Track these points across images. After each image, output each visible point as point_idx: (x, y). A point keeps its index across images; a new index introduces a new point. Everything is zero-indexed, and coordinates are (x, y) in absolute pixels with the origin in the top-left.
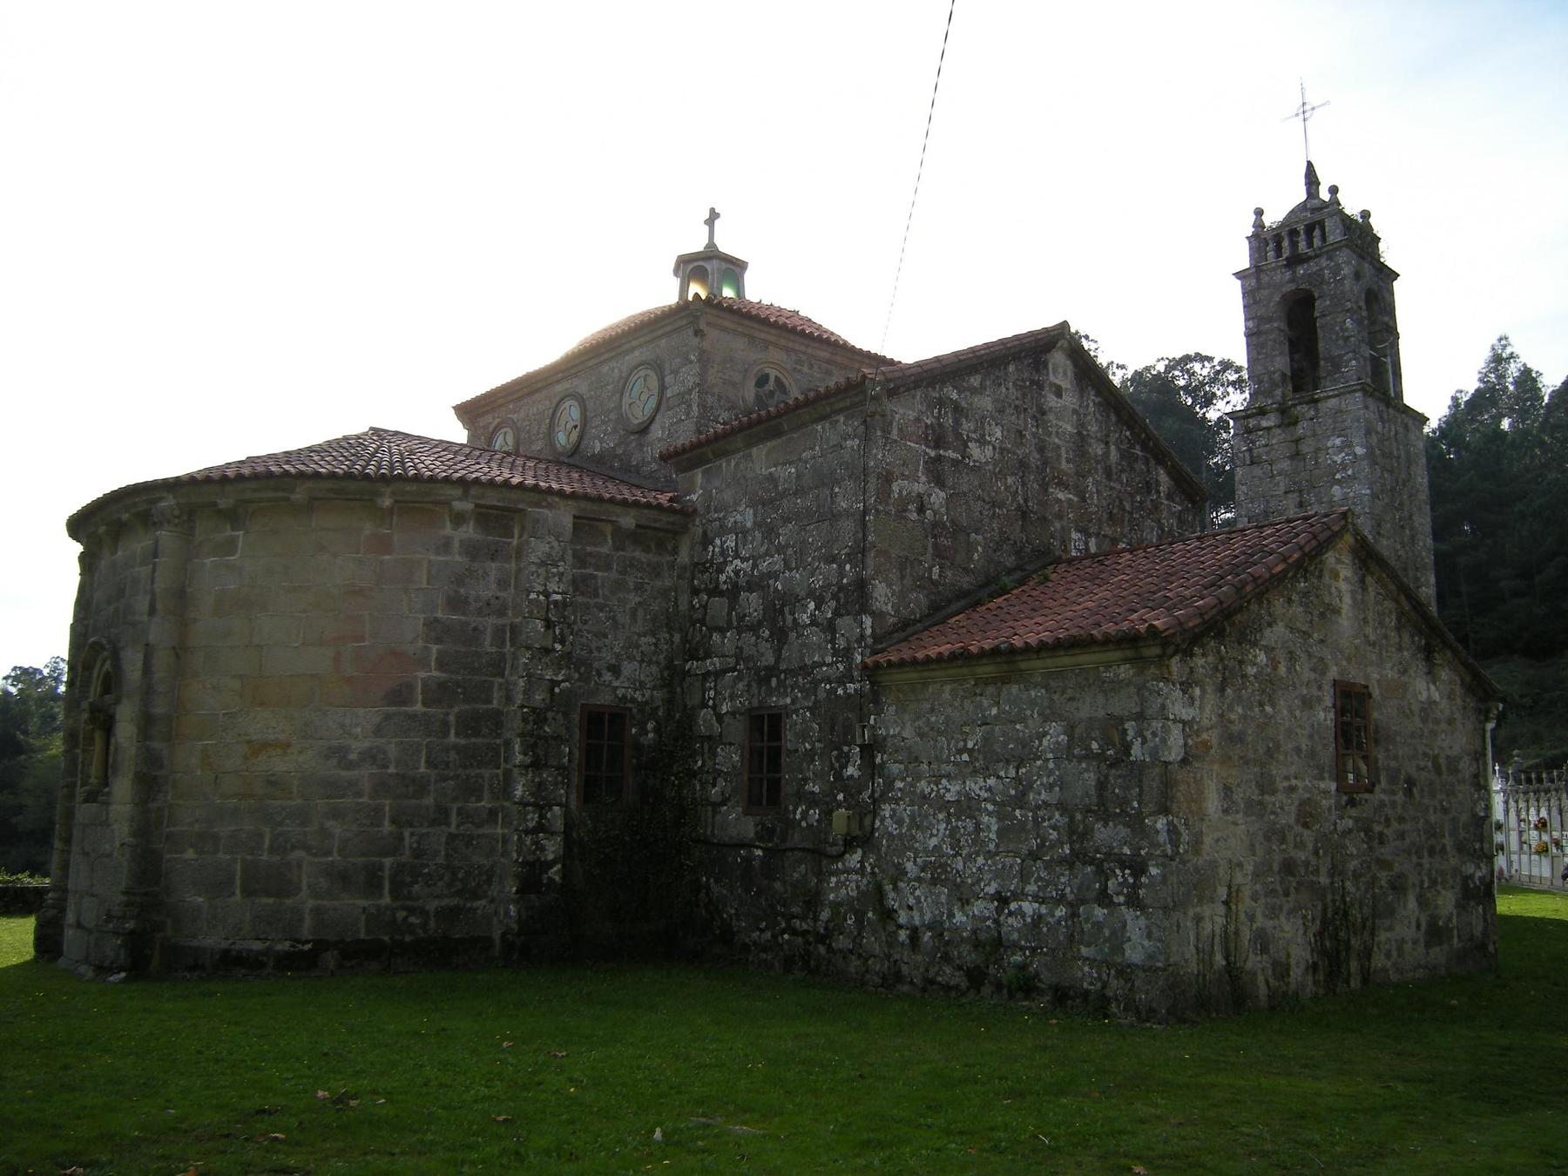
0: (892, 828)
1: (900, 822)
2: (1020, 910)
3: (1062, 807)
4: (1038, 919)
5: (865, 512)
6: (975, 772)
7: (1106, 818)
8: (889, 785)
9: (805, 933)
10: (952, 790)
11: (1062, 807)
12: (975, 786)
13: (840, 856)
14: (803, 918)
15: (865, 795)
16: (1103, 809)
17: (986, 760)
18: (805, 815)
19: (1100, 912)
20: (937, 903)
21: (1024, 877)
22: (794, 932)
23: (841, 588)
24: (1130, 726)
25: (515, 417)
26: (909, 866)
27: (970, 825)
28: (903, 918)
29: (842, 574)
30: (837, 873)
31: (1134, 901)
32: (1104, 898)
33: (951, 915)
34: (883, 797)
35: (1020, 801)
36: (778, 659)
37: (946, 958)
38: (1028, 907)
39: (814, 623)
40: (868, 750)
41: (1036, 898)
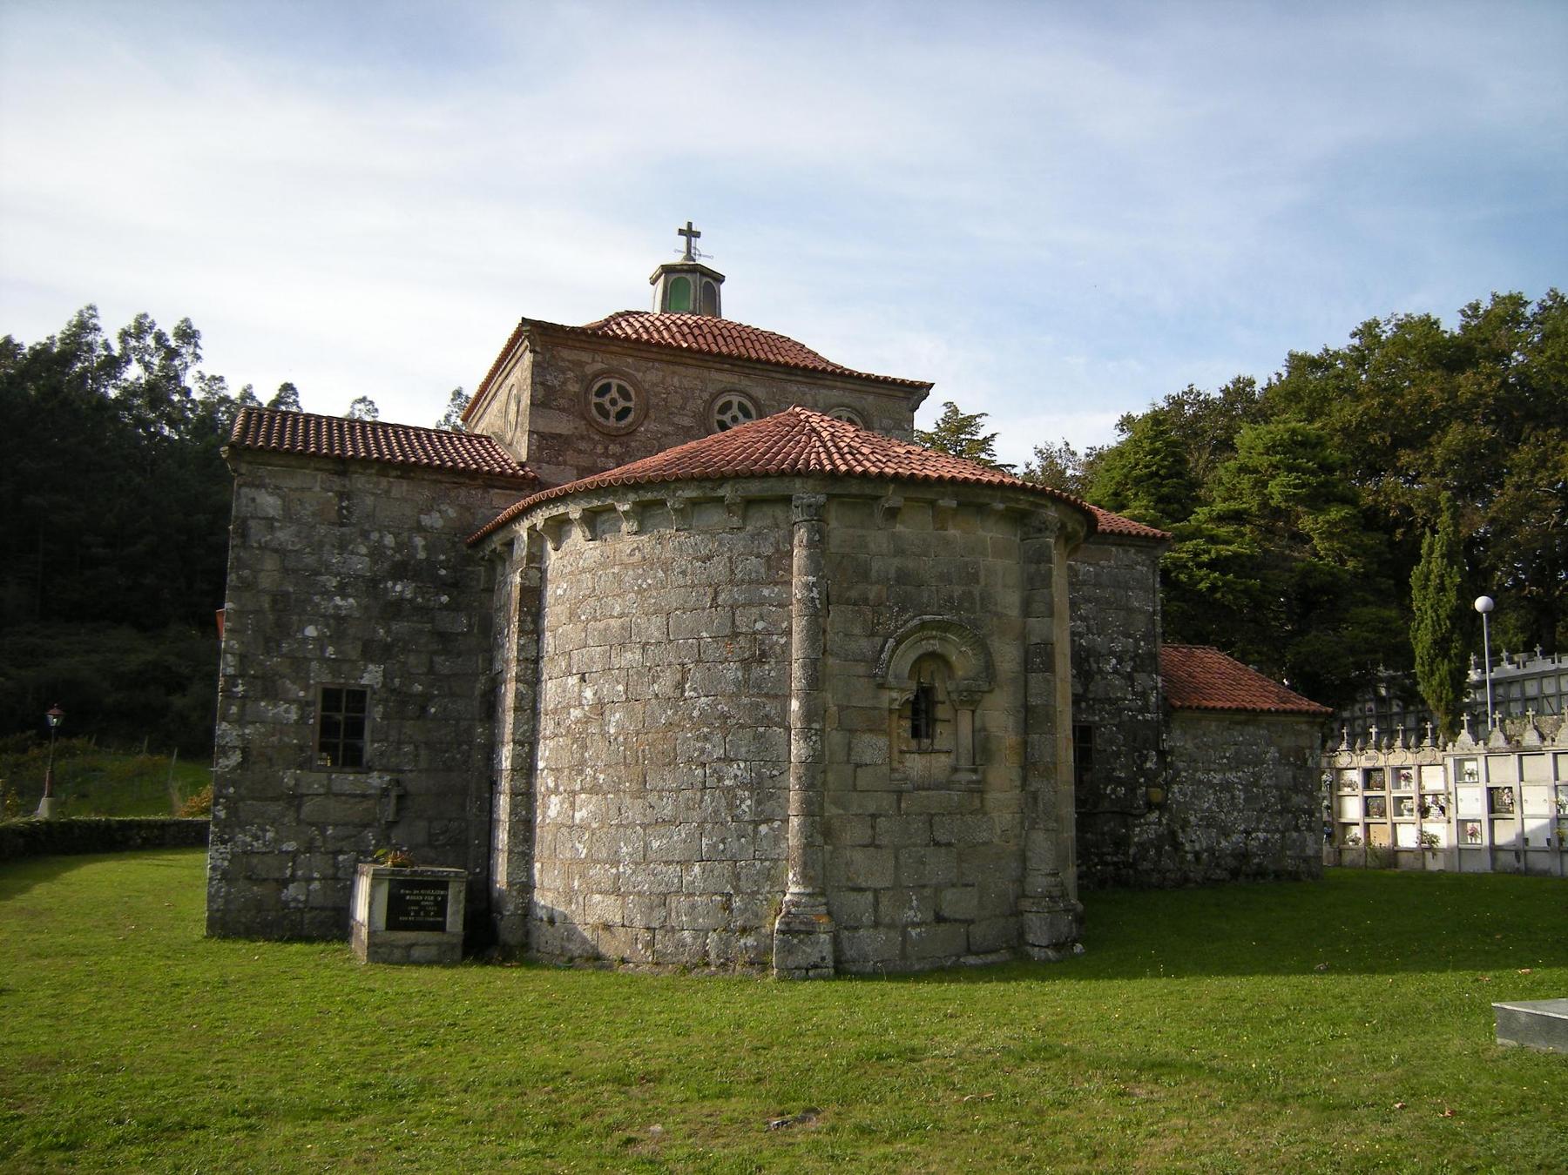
0: (1181, 799)
1: (1185, 795)
3: (1277, 787)
4: (1266, 840)
5: (1154, 613)
6: (1231, 769)
7: (1297, 792)
8: (1177, 773)
9: (1115, 864)
10: (1217, 778)
12: (1230, 776)
13: (1143, 816)
14: (1115, 854)
15: (1160, 780)
16: (1295, 789)
17: (1237, 763)
18: (1113, 791)
19: (1295, 835)
20: (1209, 837)
21: (1258, 821)
22: (1106, 864)
23: (1137, 655)
24: (1307, 752)
25: (639, 376)
26: (1192, 818)
27: (1228, 796)
28: (1188, 847)
29: (1138, 647)
30: (1139, 825)
31: (1309, 829)
33: (1219, 843)
34: (1173, 781)
36: (1086, 690)
37: (1218, 865)
38: (1261, 835)
39: (1115, 671)
40: (1162, 754)
41: (1265, 831)
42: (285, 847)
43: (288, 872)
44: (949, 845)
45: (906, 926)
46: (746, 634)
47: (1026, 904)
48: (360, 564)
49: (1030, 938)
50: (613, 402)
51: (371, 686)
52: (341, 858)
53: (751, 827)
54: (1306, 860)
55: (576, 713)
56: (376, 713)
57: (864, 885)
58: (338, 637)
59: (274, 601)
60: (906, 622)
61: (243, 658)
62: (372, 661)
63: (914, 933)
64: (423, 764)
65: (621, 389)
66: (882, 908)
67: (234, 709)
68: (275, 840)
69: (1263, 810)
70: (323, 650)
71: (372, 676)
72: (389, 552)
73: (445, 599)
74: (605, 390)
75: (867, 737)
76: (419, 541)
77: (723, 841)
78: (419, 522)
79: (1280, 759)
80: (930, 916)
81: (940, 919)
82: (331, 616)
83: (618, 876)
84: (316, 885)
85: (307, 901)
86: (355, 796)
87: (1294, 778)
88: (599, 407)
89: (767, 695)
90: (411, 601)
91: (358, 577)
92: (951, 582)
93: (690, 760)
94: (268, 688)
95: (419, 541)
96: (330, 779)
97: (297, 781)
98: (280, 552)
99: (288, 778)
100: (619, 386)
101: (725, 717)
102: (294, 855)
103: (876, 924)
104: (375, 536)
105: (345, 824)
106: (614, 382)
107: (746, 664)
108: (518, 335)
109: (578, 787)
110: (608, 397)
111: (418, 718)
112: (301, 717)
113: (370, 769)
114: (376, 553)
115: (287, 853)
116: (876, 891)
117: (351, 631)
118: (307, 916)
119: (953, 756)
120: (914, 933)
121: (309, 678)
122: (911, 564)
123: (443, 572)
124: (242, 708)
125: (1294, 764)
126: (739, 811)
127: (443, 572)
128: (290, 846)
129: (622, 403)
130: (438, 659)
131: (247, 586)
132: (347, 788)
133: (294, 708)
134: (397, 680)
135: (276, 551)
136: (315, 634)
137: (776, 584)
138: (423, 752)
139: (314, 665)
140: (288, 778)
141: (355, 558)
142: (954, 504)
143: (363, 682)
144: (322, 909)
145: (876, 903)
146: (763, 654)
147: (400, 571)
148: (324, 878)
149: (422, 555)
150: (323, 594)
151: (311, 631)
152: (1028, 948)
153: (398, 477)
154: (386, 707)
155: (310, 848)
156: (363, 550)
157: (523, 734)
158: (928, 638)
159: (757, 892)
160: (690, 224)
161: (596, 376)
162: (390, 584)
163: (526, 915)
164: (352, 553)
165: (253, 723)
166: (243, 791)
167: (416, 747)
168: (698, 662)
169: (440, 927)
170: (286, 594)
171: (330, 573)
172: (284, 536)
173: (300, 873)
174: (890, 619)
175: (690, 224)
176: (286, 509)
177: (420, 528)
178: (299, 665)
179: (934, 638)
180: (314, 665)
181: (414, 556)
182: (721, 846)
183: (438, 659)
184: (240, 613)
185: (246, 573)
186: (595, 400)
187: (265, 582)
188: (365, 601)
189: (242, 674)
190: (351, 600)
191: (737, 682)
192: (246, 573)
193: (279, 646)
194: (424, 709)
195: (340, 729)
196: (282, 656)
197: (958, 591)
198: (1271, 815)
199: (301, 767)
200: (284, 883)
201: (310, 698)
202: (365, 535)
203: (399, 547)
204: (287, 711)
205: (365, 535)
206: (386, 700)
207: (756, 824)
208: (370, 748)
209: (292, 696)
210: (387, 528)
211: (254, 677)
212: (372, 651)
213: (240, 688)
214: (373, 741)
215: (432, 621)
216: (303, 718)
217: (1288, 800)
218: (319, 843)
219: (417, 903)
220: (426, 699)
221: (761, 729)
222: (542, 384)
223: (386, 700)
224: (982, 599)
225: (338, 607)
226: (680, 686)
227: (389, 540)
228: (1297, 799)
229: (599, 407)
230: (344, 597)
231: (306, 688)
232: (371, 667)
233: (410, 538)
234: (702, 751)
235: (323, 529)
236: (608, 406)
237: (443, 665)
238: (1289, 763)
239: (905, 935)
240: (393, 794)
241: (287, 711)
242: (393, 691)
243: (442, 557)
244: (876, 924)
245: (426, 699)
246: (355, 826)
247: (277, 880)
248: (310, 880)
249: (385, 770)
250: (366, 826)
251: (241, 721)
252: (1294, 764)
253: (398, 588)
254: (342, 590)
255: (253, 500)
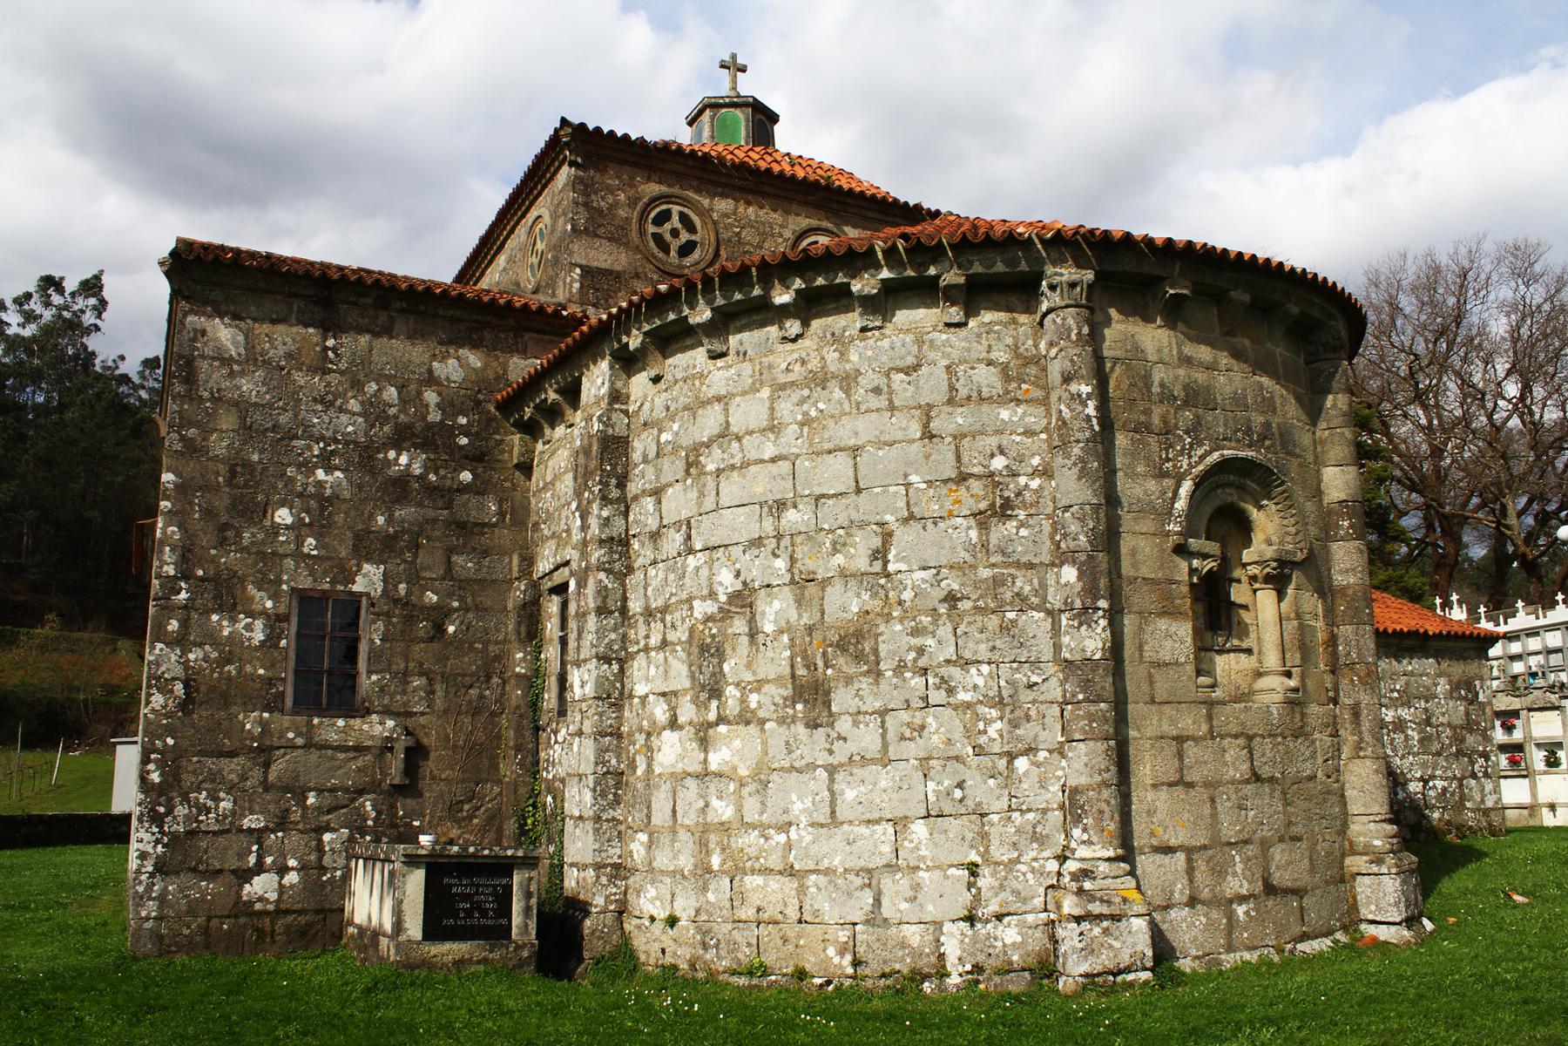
2: (1435, 787)
4: (1445, 789)
7: (1471, 731)
11: (1449, 725)
12: (1404, 713)
17: (1406, 700)
31: (1486, 775)
32: (1474, 776)
35: (1428, 722)
38: (1439, 784)
42: (246, 823)
43: (252, 860)
44: (1272, 780)
45: (1231, 901)
46: (978, 477)
47: (1355, 863)
48: (350, 426)
49: (1367, 912)
50: (675, 233)
51: (368, 595)
52: (327, 837)
53: (1004, 761)
54: (1486, 812)
55: (702, 608)
56: (372, 634)
57: (1173, 842)
58: (320, 527)
59: (233, 473)
60: (1202, 458)
61: (186, 557)
62: (368, 560)
63: (1241, 910)
64: (439, 703)
65: (684, 218)
66: (1198, 876)
67: (174, 625)
68: (233, 813)
69: (1438, 754)
70: (300, 542)
71: (369, 579)
72: (393, 411)
73: (466, 476)
74: (664, 217)
75: (1163, 624)
76: (431, 397)
77: (960, 785)
78: (430, 371)
79: (1451, 691)
80: (1259, 887)
81: (1270, 889)
82: (311, 496)
83: (789, 846)
84: (292, 878)
85: (278, 901)
86: (347, 749)
87: (1467, 714)
88: (658, 238)
89: (1018, 565)
90: (422, 478)
91: (347, 443)
92: (1246, 409)
93: (900, 668)
94: (225, 594)
95: (431, 397)
96: (310, 723)
97: (264, 724)
98: (241, 406)
99: (250, 723)
100: (682, 214)
101: (951, 599)
102: (258, 835)
103: (1192, 902)
104: (372, 387)
105: (332, 790)
106: (676, 209)
107: (983, 519)
108: (554, 144)
109: (712, 716)
110: (667, 226)
111: (431, 640)
112: (268, 638)
113: (368, 712)
114: (374, 412)
115: (251, 831)
116: (1189, 851)
117: (340, 518)
118: (280, 925)
119: (1254, 658)
120: (1241, 910)
121: (281, 582)
122: (1200, 377)
123: (464, 441)
124: (185, 623)
125: (1465, 698)
126: (983, 740)
127: (464, 441)
128: (251, 821)
129: (685, 236)
130: (458, 559)
131: (192, 449)
132: (333, 737)
133: (259, 624)
134: (402, 586)
135: (236, 404)
136: (289, 520)
137: (1018, 402)
138: (440, 689)
139: (289, 563)
140: (250, 723)
141: (344, 418)
142: (1247, 298)
143: (356, 588)
144: (300, 912)
145: (1190, 871)
146: (1007, 504)
147: (403, 437)
148: (302, 868)
149: (435, 416)
150: (299, 466)
151: (283, 516)
152: (1363, 927)
153: (401, 311)
154: (388, 623)
155: (282, 823)
156: (354, 405)
157: (609, 646)
158: (1223, 486)
159: (1017, 861)
160: (734, 56)
161: (655, 200)
162: (392, 454)
163: (621, 913)
164: (341, 410)
165: (200, 645)
166: (185, 743)
167: (431, 681)
168: (906, 521)
169: (502, 933)
170: (247, 464)
171: (311, 437)
172: (248, 386)
173: (269, 860)
174: (1182, 453)
175: (734, 56)
176: (250, 346)
177: (431, 380)
178: (267, 562)
179: (1230, 485)
180: (289, 563)
181: (424, 418)
182: (958, 794)
183: (458, 559)
184: (182, 488)
185: (192, 432)
186: (651, 229)
187: (219, 446)
188: (357, 476)
189: (186, 575)
190: (338, 474)
191: (970, 548)
192: (192, 432)
193: (239, 535)
194: (440, 629)
195: (324, 663)
196: (242, 550)
197: (1258, 419)
198: (1446, 759)
199: (268, 708)
200: (246, 875)
201: (282, 609)
202: (357, 385)
203: (404, 402)
204: (249, 628)
205: (357, 385)
206: (388, 615)
207: (1011, 757)
208: (368, 681)
209: (257, 607)
210: (390, 379)
211: (202, 579)
212: (367, 547)
213: (183, 595)
214: (370, 673)
215: (449, 506)
216: (272, 640)
217: (1462, 740)
218: (296, 816)
219: (466, 897)
220: (439, 616)
221: (1011, 615)
222: (586, 205)
223: (388, 615)
224: (1281, 435)
225: (320, 484)
226: (880, 554)
227: (391, 393)
228: (1471, 740)
229: (658, 238)
230: (329, 470)
231: (275, 596)
232: (367, 567)
233: (419, 394)
234: (921, 651)
235: (300, 378)
236: (668, 237)
237: (465, 564)
238: (1460, 698)
239: (1231, 916)
240: (400, 747)
241: (249, 628)
242: (396, 601)
243: (463, 421)
244: (1192, 902)
245: (439, 616)
246: (346, 790)
247: (234, 872)
248: (282, 870)
249: (387, 712)
250: (361, 792)
251: (181, 642)
252: (1465, 698)
253: (404, 459)
254: (326, 461)
255: (204, 333)
